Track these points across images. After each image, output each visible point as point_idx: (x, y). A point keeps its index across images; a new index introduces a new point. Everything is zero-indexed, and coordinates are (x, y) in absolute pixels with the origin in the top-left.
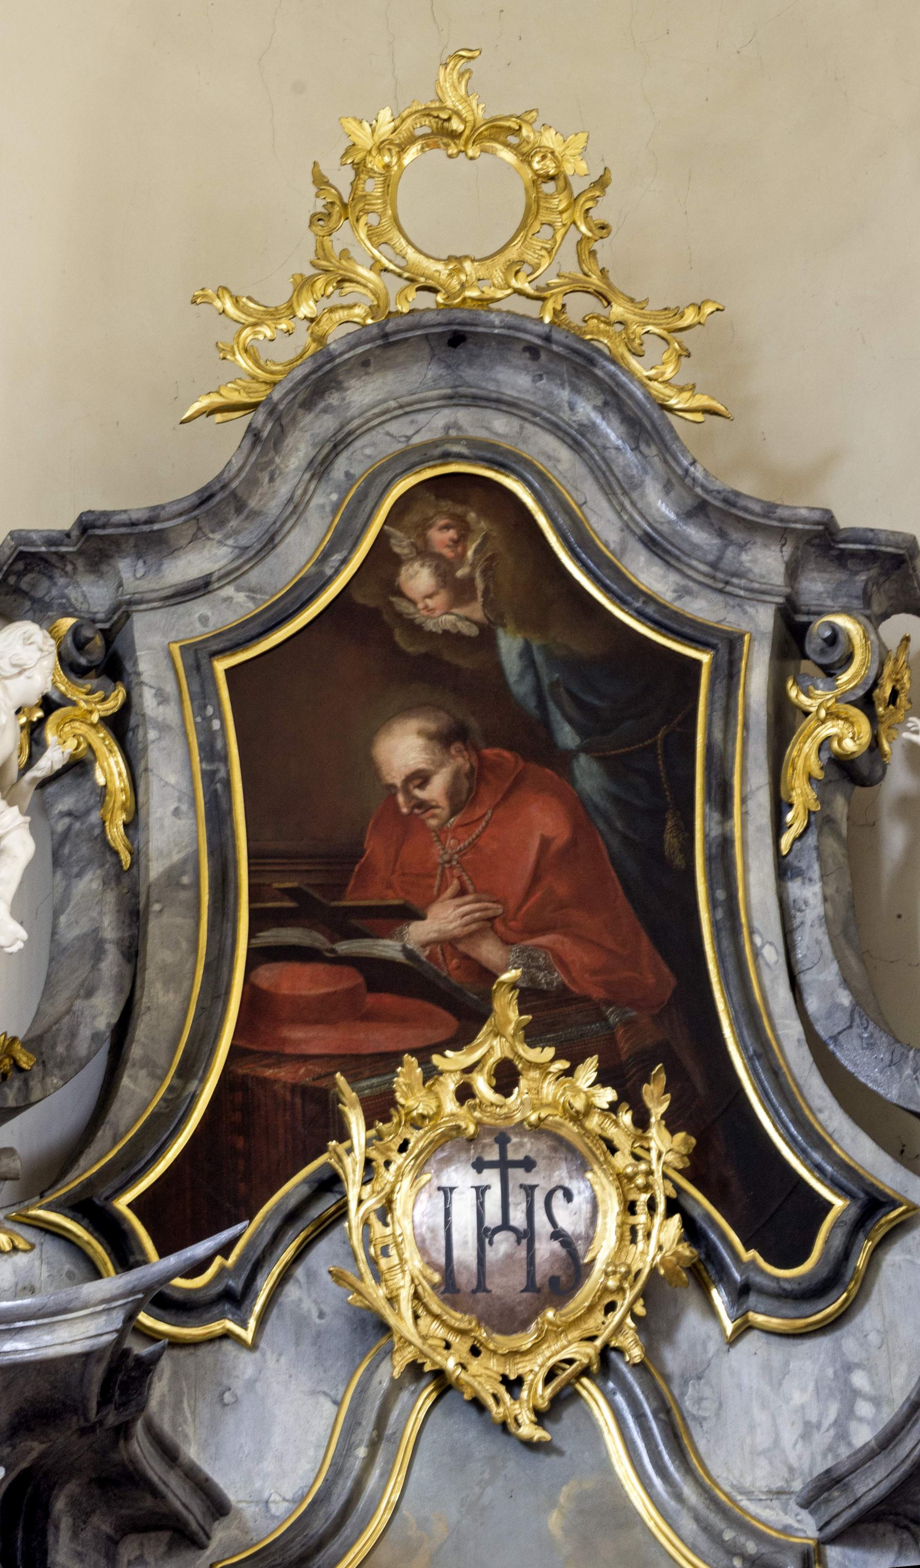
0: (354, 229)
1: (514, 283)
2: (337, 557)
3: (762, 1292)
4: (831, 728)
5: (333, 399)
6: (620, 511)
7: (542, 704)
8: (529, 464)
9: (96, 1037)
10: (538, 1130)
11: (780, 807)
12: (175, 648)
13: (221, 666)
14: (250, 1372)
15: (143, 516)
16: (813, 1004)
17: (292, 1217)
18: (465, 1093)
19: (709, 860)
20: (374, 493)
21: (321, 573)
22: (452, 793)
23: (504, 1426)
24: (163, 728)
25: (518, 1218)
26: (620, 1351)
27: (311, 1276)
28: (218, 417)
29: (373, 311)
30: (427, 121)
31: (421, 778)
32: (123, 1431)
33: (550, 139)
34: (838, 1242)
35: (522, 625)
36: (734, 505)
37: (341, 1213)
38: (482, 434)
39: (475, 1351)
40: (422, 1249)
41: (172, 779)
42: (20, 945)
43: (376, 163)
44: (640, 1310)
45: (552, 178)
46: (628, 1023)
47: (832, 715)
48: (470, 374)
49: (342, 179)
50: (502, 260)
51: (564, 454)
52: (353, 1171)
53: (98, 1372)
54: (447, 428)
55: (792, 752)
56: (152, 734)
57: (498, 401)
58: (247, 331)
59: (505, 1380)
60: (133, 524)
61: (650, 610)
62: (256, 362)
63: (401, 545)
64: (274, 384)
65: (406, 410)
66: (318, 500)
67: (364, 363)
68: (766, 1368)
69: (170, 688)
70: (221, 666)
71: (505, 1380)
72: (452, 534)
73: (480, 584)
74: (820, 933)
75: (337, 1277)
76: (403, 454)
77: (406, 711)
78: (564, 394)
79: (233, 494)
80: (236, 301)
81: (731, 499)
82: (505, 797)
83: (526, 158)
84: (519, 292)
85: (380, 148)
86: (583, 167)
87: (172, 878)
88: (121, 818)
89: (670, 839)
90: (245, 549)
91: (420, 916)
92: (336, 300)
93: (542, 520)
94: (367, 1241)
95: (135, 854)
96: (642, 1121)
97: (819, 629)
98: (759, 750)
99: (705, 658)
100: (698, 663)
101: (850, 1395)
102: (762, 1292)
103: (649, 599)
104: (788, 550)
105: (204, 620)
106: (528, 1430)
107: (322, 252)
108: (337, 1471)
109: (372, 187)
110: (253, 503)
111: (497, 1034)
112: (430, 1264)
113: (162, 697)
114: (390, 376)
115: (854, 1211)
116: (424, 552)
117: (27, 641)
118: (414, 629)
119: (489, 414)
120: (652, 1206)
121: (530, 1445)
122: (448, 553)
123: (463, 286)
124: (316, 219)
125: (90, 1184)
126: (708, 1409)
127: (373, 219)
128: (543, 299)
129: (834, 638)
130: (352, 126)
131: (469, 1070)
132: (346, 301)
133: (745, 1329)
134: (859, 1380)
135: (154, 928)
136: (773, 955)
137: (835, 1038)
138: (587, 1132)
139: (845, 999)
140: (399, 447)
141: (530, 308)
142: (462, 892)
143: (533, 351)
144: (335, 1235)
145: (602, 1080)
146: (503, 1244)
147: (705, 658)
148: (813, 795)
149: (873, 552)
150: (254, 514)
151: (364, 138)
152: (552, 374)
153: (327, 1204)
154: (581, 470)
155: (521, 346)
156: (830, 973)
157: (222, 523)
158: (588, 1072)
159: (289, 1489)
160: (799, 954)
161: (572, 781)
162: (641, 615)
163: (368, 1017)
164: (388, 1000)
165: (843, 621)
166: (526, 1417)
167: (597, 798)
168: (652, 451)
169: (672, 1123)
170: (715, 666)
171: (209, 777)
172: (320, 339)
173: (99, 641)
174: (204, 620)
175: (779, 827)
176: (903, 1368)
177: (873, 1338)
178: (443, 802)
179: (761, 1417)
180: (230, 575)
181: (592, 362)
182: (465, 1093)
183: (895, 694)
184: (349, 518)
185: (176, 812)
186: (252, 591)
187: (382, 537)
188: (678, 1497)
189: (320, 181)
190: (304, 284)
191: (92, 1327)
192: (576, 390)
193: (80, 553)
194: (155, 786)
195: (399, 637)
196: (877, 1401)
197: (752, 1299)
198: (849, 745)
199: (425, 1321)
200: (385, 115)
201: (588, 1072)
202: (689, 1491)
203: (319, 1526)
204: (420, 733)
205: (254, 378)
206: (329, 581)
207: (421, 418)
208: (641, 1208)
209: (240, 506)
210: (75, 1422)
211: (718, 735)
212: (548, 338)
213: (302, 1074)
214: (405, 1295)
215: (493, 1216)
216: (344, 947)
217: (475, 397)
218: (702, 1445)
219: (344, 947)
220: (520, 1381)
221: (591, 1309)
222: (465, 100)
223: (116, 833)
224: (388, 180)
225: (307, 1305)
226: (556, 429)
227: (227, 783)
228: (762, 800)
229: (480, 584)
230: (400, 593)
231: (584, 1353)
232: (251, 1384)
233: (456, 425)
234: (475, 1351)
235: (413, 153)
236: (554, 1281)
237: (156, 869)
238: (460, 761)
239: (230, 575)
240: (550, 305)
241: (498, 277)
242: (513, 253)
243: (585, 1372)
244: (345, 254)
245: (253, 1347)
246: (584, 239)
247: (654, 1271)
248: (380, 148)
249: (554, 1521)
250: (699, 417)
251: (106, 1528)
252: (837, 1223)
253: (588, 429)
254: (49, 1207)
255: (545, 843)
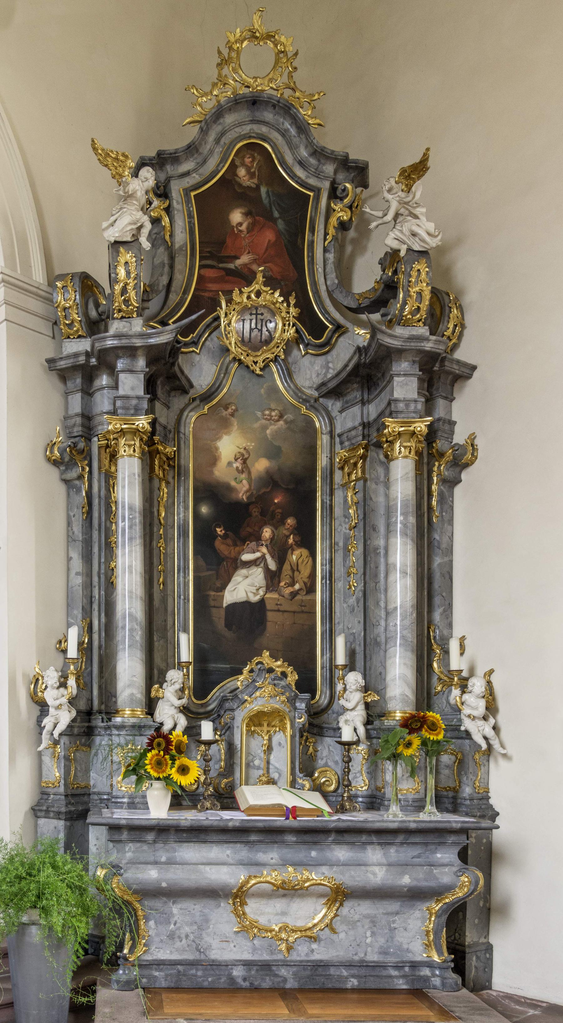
0: (229, 68)
1: (271, 85)
2: (222, 165)
3: (312, 345)
4: (340, 214)
5: (221, 120)
6: (293, 154)
7: (270, 204)
8: (271, 139)
9: (163, 285)
10: (265, 307)
11: (326, 234)
12: (181, 190)
13: (193, 194)
14: (198, 359)
15: (173, 151)
16: (328, 283)
17: (208, 326)
18: (249, 297)
19: (308, 246)
20: (231, 147)
21: (217, 169)
22: (248, 228)
23: (253, 372)
24: (178, 211)
25: (259, 327)
26: (279, 356)
27: (212, 340)
28: (192, 125)
29: (233, 93)
30: (249, 33)
31: (240, 224)
32: (173, 364)
33: (283, 39)
34: (330, 335)
35: (267, 185)
36: (323, 151)
37: (219, 325)
38: (259, 132)
39: (248, 355)
40: (237, 332)
41: (181, 224)
42: (149, 248)
43: (235, 47)
44: (284, 347)
45: (283, 52)
46: (286, 285)
47: (342, 210)
48: (257, 114)
49: (225, 52)
50: (267, 78)
51: (280, 138)
52: (223, 316)
53: (169, 348)
54: (250, 130)
55: (330, 220)
56: (176, 212)
57: (264, 122)
58: (200, 99)
59: (254, 362)
60: (171, 154)
61: (299, 181)
62: (202, 108)
63: (237, 163)
64: (206, 115)
65: (240, 124)
66: (217, 150)
67: (230, 109)
68: (311, 362)
69: (180, 200)
70: (193, 194)
71: (254, 362)
72: (250, 159)
73: (257, 173)
74: (332, 266)
75: (218, 338)
76: (239, 136)
77: (237, 207)
78: (282, 120)
79: (196, 147)
80: (197, 90)
81: (323, 149)
82: (260, 230)
83: (276, 45)
84: (272, 88)
85: (236, 42)
86: (291, 49)
87: (181, 248)
88: (168, 233)
89: (299, 241)
90: (198, 163)
91: (239, 258)
92: (223, 90)
93: (274, 156)
94: (225, 330)
95: (172, 243)
96: (289, 305)
97: (341, 187)
98: (322, 219)
99: (312, 194)
100: (310, 196)
101: (328, 368)
102: (312, 345)
103: (299, 178)
104: (335, 165)
105: (188, 183)
106: (258, 372)
107: (220, 75)
108: (217, 379)
109: (234, 55)
110: (201, 150)
111: (257, 283)
112: (239, 336)
113: (178, 203)
114: (236, 114)
115: (334, 328)
116: (243, 164)
117: (148, 171)
118: (240, 185)
119: (261, 126)
120: (289, 324)
121: (258, 375)
122: (249, 165)
123: (257, 86)
124: (218, 65)
125: (163, 317)
126: (297, 370)
127: (233, 65)
128: (278, 90)
129: (345, 189)
130: (229, 34)
131: (250, 292)
132: (226, 90)
133: (307, 353)
134: (331, 365)
135: (177, 260)
136: (321, 270)
137: (333, 291)
138: (276, 307)
139: (336, 281)
140: (237, 135)
141: (274, 93)
142: (249, 253)
143: (274, 106)
144: (217, 331)
145: (280, 296)
146: (255, 332)
147: (311, 194)
148: (334, 231)
149: (357, 166)
150: (201, 154)
151: (232, 39)
152: (278, 113)
153: (216, 323)
154: (284, 142)
155: (271, 105)
156: (334, 275)
157: (193, 155)
158: (277, 294)
159: (206, 383)
160: (327, 270)
161: (277, 226)
162: (297, 182)
163: (226, 282)
164: (230, 278)
165: (348, 185)
166: (258, 369)
167: (283, 231)
168: (303, 136)
169: (295, 306)
170: (314, 196)
171: (190, 223)
172: (218, 102)
173: (162, 187)
174: (188, 183)
175: (325, 239)
176: (340, 363)
177: (335, 356)
178: (245, 230)
179: (308, 372)
180: (195, 170)
181: (290, 109)
182: (249, 297)
183: (357, 205)
184: (225, 155)
185: (182, 232)
186: (200, 175)
187: (233, 160)
188: (289, 386)
189: (219, 52)
190: (214, 85)
191: (168, 336)
192: (284, 119)
193: (157, 163)
194: (176, 226)
195: (236, 188)
196: (334, 370)
197: (309, 347)
198: (345, 218)
199: (237, 348)
200: (238, 30)
201: (277, 294)
202: (292, 385)
203: (213, 390)
204: (241, 213)
205: (201, 113)
206: (219, 171)
207: (244, 127)
208: (287, 325)
209: (197, 151)
210: (163, 362)
211: (313, 214)
212: (279, 102)
213: (210, 295)
214: (233, 342)
215: (253, 326)
216: (221, 265)
217: (258, 121)
218: (295, 377)
219: (221, 265)
220: (257, 362)
221: (274, 347)
222: (260, 26)
223: (167, 238)
224: (238, 52)
225: (211, 346)
226: (278, 130)
227: (194, 224)
228: (322, 231)
229: (257, 173)
230: (237, 176)
231: (271, 356)
232: (199, 361)
233: (253, 129)
234: (248, 355)
235: (245, 43)
236: (266, 341)
237: (177, 246)
238: (250, 220)
239: (195, 170)
240: (280, 92)
241: (266, 83)
242: (270, 76)
243: (271, 361)
244: (226, 76)
245: (199, 354)
246: (290, 72)
247: (288, 339)
248: (236, 42)
249: (262, 391)
250: (316, 126)
251: (168, 389)
252: (330, 331)
253: (287, 130)
254: (154, 322)
255: (269, 241)
